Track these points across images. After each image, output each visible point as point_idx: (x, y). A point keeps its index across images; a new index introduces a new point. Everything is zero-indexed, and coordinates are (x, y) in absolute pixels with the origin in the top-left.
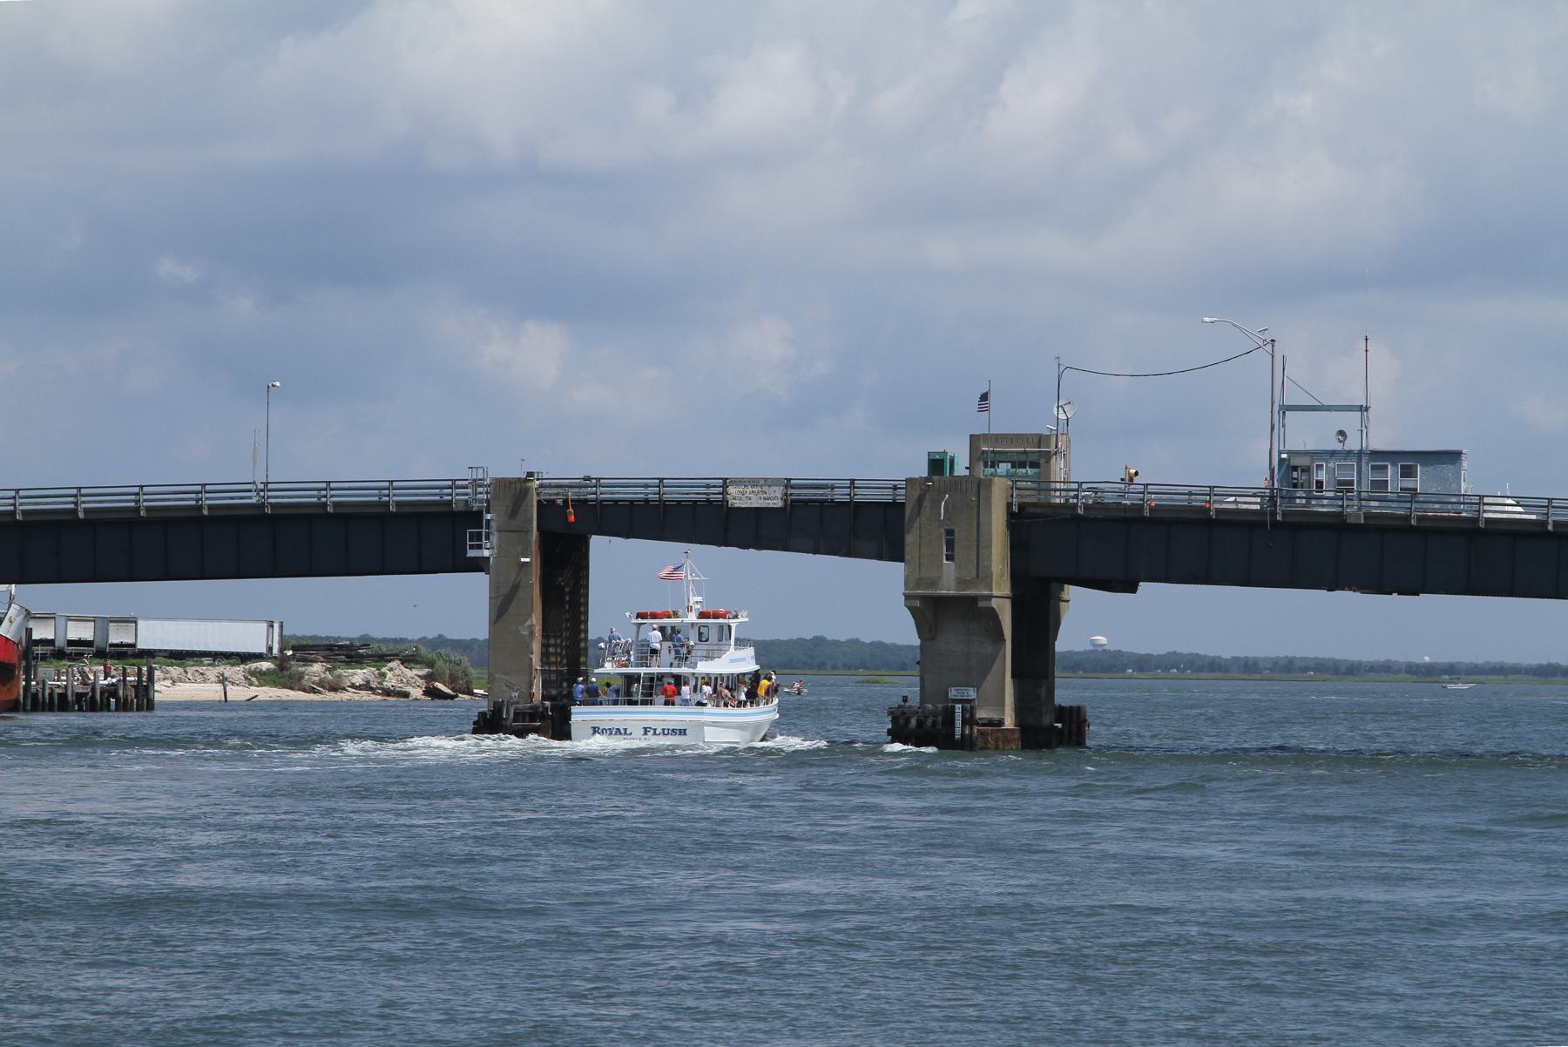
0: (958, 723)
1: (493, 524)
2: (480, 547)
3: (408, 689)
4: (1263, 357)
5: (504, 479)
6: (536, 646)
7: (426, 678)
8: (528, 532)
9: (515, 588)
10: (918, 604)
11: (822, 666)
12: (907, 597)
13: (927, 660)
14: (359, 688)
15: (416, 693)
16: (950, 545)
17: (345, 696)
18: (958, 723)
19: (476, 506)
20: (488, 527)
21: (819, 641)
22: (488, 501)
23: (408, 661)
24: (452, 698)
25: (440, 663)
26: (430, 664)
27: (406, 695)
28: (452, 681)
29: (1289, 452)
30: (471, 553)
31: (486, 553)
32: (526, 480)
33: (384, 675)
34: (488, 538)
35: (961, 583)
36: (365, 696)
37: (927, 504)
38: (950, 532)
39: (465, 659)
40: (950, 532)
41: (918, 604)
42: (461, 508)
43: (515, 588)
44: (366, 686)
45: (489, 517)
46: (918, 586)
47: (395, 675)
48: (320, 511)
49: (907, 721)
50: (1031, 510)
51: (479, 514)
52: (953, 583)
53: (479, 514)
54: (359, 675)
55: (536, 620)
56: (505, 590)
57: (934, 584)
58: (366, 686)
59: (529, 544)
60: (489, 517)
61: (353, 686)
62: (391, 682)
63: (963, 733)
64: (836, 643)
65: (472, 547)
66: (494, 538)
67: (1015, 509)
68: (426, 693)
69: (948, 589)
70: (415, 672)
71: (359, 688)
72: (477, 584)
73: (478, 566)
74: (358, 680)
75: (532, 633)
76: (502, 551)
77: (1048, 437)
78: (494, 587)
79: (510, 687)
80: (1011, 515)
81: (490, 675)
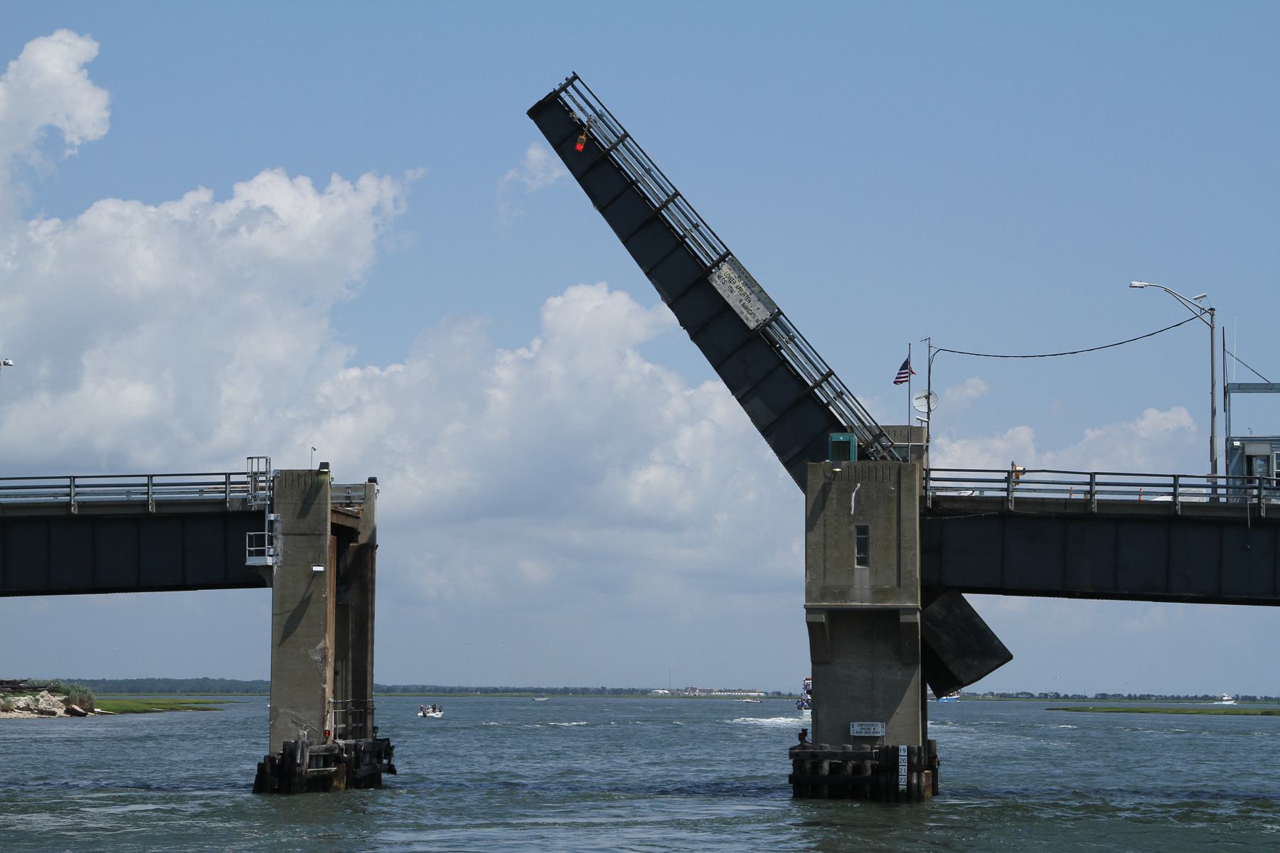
0: (903, 770)
1: (278, 526)
2: (262, 553)
3: (55, 709)
4: (1201, 328)
5: (291, 472)
6: (329, 673)
7: (66, 702)
8: (321, 534)
9: (306, 602)
10: (823, 618)
11: (208, 691)
12: (809, 610)
13: (821, 693)
14: (23, 709)
15: (60, 712)
16: (863, 546)
17: (14, 715)
18: (903, 770)
19: (255, 505)
20: (271, 530)
21: (206, 679)
22: (271, 499)
23: (54, 690)
24: (84, 715)
25: (73, 693)
26: (67, 693)
27: (54, 713)
28: (81, 704)
29: (1241, 439)
30: (252, 561)
31: (270, 561)
32: (319, 473)
33: (37, 700)
34: (271, 543)
35: (878, 592)
36: (27, 714)
37: (833, 495)
38: (862, 530)
39: (89, 689)
40: (862, 530)
41: (823, 618)
42: (237, 507)
43: (306, 602)
44: (27, 708)
45: (272, 517)
46: (823, 597)
47: (46, 700)
48: (62, 512)
49: (817, 766)
50: (946, 505)
51: (260, 514)
52: (867, 593)
53: (260, 514)
54: (22, 701)
55: (329, 641)
56: (292, 605)
57: (843, 594)
58: (27, 708)
59: (321, 549)
60: (272, 517)
61: (18, 708)
62: (43, 705)
63: (909, 783)
64: (213, 680)
65: (251, 554)
66: (279, 543)
67: (929, 504)
68: (66, 712)
69: (861, 599)
70: (57, 698)
71: (23, 709)
72: (255, 605)
73: (257, 579)
74: (21, 704)
75: (325, 658)
76: (287, 561)
77: (920, 429)
78: (278, 603)
79: (298, 723)
80: (925, 512)
81: (273, 709)
